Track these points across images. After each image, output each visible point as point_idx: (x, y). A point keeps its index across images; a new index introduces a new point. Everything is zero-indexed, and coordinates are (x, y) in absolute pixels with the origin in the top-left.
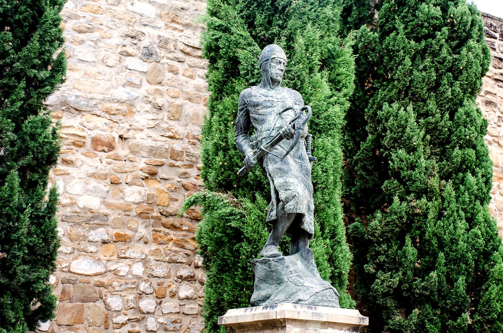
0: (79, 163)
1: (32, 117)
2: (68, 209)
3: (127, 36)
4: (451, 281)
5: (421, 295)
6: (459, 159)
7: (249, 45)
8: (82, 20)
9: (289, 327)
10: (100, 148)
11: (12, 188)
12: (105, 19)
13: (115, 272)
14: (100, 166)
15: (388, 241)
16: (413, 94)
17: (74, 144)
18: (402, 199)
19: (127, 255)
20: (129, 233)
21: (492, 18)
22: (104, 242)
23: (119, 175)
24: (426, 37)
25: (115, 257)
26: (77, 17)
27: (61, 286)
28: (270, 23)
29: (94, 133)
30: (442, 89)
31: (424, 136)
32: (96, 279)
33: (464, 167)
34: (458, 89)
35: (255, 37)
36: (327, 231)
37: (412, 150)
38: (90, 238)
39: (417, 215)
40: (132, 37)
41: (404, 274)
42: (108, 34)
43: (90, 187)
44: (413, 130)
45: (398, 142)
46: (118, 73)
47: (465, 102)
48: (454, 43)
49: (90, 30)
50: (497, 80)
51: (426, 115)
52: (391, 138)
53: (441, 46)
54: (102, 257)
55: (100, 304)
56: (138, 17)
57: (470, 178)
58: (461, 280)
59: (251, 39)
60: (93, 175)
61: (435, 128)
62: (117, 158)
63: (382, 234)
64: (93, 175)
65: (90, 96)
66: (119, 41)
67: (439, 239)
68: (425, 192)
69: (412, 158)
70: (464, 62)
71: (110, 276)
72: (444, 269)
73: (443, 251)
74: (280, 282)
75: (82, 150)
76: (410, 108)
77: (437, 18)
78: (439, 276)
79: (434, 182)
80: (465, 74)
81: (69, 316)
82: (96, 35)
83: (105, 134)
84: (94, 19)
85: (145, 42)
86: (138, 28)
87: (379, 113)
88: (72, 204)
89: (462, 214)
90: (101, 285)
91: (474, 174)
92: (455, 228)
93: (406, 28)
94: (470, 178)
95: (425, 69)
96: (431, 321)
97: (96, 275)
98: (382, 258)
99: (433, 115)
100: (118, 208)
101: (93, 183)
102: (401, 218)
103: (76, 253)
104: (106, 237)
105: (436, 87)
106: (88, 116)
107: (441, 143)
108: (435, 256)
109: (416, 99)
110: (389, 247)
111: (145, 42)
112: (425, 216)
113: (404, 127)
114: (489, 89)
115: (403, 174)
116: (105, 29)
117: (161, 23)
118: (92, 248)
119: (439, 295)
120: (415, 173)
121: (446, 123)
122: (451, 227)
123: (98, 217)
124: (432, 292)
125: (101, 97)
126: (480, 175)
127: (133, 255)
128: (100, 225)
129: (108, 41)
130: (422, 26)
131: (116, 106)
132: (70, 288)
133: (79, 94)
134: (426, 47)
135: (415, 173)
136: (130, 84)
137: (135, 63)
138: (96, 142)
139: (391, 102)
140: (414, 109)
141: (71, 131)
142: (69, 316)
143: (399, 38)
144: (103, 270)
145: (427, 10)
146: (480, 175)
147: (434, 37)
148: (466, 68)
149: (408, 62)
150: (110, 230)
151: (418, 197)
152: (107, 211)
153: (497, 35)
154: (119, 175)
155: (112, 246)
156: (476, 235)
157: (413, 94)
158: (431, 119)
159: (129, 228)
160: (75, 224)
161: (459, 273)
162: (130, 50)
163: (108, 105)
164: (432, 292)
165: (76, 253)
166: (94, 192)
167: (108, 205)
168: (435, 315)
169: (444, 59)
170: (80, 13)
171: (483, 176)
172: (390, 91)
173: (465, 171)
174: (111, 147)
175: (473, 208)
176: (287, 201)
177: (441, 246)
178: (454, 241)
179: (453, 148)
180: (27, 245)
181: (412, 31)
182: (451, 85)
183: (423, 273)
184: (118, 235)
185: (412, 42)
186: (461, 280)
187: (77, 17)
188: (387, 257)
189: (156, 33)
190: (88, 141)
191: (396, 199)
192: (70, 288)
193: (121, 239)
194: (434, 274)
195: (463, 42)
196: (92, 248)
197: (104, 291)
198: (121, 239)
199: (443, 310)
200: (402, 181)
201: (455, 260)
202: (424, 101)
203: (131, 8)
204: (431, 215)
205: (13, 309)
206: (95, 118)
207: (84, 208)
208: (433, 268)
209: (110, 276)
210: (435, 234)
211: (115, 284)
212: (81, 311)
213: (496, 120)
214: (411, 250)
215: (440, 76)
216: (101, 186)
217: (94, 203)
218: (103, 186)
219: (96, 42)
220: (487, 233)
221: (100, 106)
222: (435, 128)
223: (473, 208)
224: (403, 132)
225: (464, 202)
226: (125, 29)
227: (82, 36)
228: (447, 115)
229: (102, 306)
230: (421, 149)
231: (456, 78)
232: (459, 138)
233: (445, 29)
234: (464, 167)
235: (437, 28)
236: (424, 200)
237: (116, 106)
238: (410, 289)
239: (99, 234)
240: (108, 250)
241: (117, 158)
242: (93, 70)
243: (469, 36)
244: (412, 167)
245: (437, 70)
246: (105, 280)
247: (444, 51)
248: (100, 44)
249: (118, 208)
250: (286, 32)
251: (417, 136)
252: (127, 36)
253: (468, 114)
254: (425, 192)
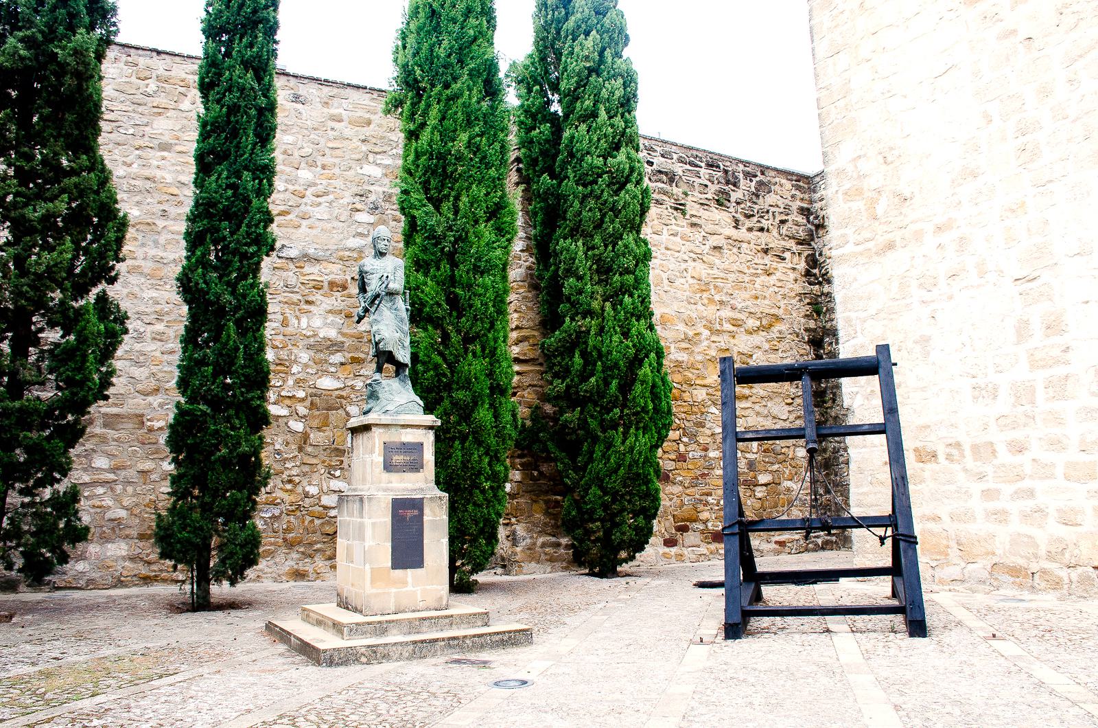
0: (318, 303)
1: (243, 282)
2: (312, 340)
3: (356, 195)
4: (607, 384)
5: (584, 396)
6: (619, 284)
7: (425, 206)
8: (319, 187)
9: (374, 429)
10: (335, 289)
11: (229, 336)
12: (338, 183)
13: (352, 387)
14: (336, 304)
15: (561, 354)
16: (583, 231)
17: (314, 287)
18: (572, 319)
19: (361, 373)
20: (362, 356)
21: (697, 150)
22: (342, 364)
23: (352, 310)
24: (592, 183)
25: (352, 375)
26: (315, 184)
27: (310, 399)
28: (443, 186)
29: (330, 278)
30: (604, 226)
31: (591, 266)
32: (337, 392)
33: (624, 290)
34: (617, 225)
35: (428, 199)
36: (487, 351)
37: (580, 278)
38: (331, 361)
39: (583, 332)
40: (361, 196)
41: (572, 380)
42: (340, 196)
43: (328, 321)
44: (581, 262)
45: (570, 272)
46: (349, 227)
47: (625, 236)
48: (615, 187)
49: (326, 194)
50: (702, 204)
51: (593, 248)
52: (564, 269)
53: (602, 191)
54: (340, 376)
55: (341, 412)
56: (366, 178)
57: (627, 299)
58: (614, 383)
59: (426, 201)
60: (330, 312)
61: (600, 259)
62: (350, 296)
63: (556, 350)
64: (330, 312)
65: (326, 248)
66: (351, 200)
67: (599, 351)
68: (589, 313)
69: (580, 285)
70: (622, 203)
71: (348, 390)
72: (602, 375)
73: (601, 361)
74: (378, 398)
75: (321, 292)
76: (580, 243)
77: (599, 168)
78: (597, 381)
79: (595, 305)
80: (623, 212)
81: (317, 421)
82: (331, 197)
83: (339, 278)
84: (329, 184)
85: (372, 198)
86: (366, 187)
87: (558, 247)
88: (315, 335)
89: (618, 329)
90: (341, 397)
91: (631, 295)
92: (611, 341)
93: (575, 176)
94: (627, 299)
95: (590, 210)
96: (592, 416)
97: (337, 390)
98: (557, 369)
99: (598, 248)
100: (352, 336)
101: (331, 318)
102: (571, 335)
103: (320, 373)
104: (343, 360)
105: (599, 225)
106: (325, 264)
107: (604, 270)
108: (595, 365)
109: (588, 236)
110: (563, 359)
111: (372, 198)
112: (588, 332)
113: (574, 259)
114: (694, 213)
115: (573, 298)
116: (339, 191)
117: (386, 181)
118: (333, 369)
119: (598, 395)
120: (582, 298)
121: (609, 253)
122: (608, 341)
123: (336, 344)
124: (591, 394)
125: (336, 247)
126: (636, 296)
127: (366, 373)
128: (338, 351)
129: (341, 201)
130: (587, 175)
131: (347, 253)
132: (317, 400)
133: (318, 246)
134: (592, 191)
135: (582, 298)
136: (360, 235)
137: (363, 217)
138: (332, 284)
139: (565, 238)
140: (583, 244)
141: (312, 277)
142: (317, 421)
143: (569, 185)
144: (342, 386)
145: (590, 161)
146: (636, 296)
147: (597, 183)
148: (624, 207)
149: (577, 204)
150: (346, 354)
151: (584, 318)
152: (341, 339)
153: (703, 165)
154: (352, 310)
155: (348, 367)
156: (628, 347)
157: (583, 231)
158: (596, 252)
159: (362, 352)
160: (318, 351)
161: (613, 378)
162: (359, 206)
163: (341, 253)
164: (591, 394)
165: (320, 373)
166: (332, 324)
167: (343, 335)
168: (595, 411)
169: (606, 201)
170: (318, 182)
171: (639, 296)
172: (565, 229)
173: (624, 294)
174: (344, 288)
175: (629, 324)
176: (380, 341)
177: (600, 356)
178: (609, 352)
179: (615, 274)
180: (243, 375)
181: (580, 179)
182: (612, 222)
183: (584, 378)
184: (352, 358)
185: (580, 188)
186: (614, 383)
187: (315, 184)
188: (561, 367)
189: (381, 189)
190: (326, 285)
191: (568, 319)
192: (317, 400)
193: (355, 360)
194: (593, 380)
195: (622, 186)
196: (333, 369)
197: (344, 402)
198: (355, 360)
199: (602, 407)
200: (573, 304)
201: (611, 368)
202: (592, 236)
203: (360, 171)
204: (592, 333)
205: (238, 418)
206: (331, 265)
207: (324, 338)
208: (592, 375)
209: (348, 390)
210: (595, 347)
211: (352, 396)
212: (327, 417)
213: (701, 240)
214: (578, 360)
215: (603, 216)
216: (337, 320)
217: (332, 333)
218: (339, 320)
219: (330, 203)
220: (640, 343)
221: (334, 255)
222: (600, 259)
223: (629, 324)
224: (573, 263)
225: (620, 320)
226: (355, 190)
227: (320, 200)
228: (610, 248)
229: (344, 413)
230: (588, 277)
231: (616, 217)
232: (619, 267)
233: (605, 176)
234: (624, 290)
235: (600, 176)
236: (588, 320)
237: (347, 253)
238: (577, 393)
239: (337, 358)
240: (345, 370)
241: (350, 296)
242: (329, 226)
243: (628, 180)
244: (580, 292)
245: (600, 210)
246: (344, 394)
247: (605, 194)
248: (334, 204)
249: (352, 336)
250: (453, 193)
251: (583, 265)
252: (356, 195)
253: (626, 246)
254: (589, 313)
